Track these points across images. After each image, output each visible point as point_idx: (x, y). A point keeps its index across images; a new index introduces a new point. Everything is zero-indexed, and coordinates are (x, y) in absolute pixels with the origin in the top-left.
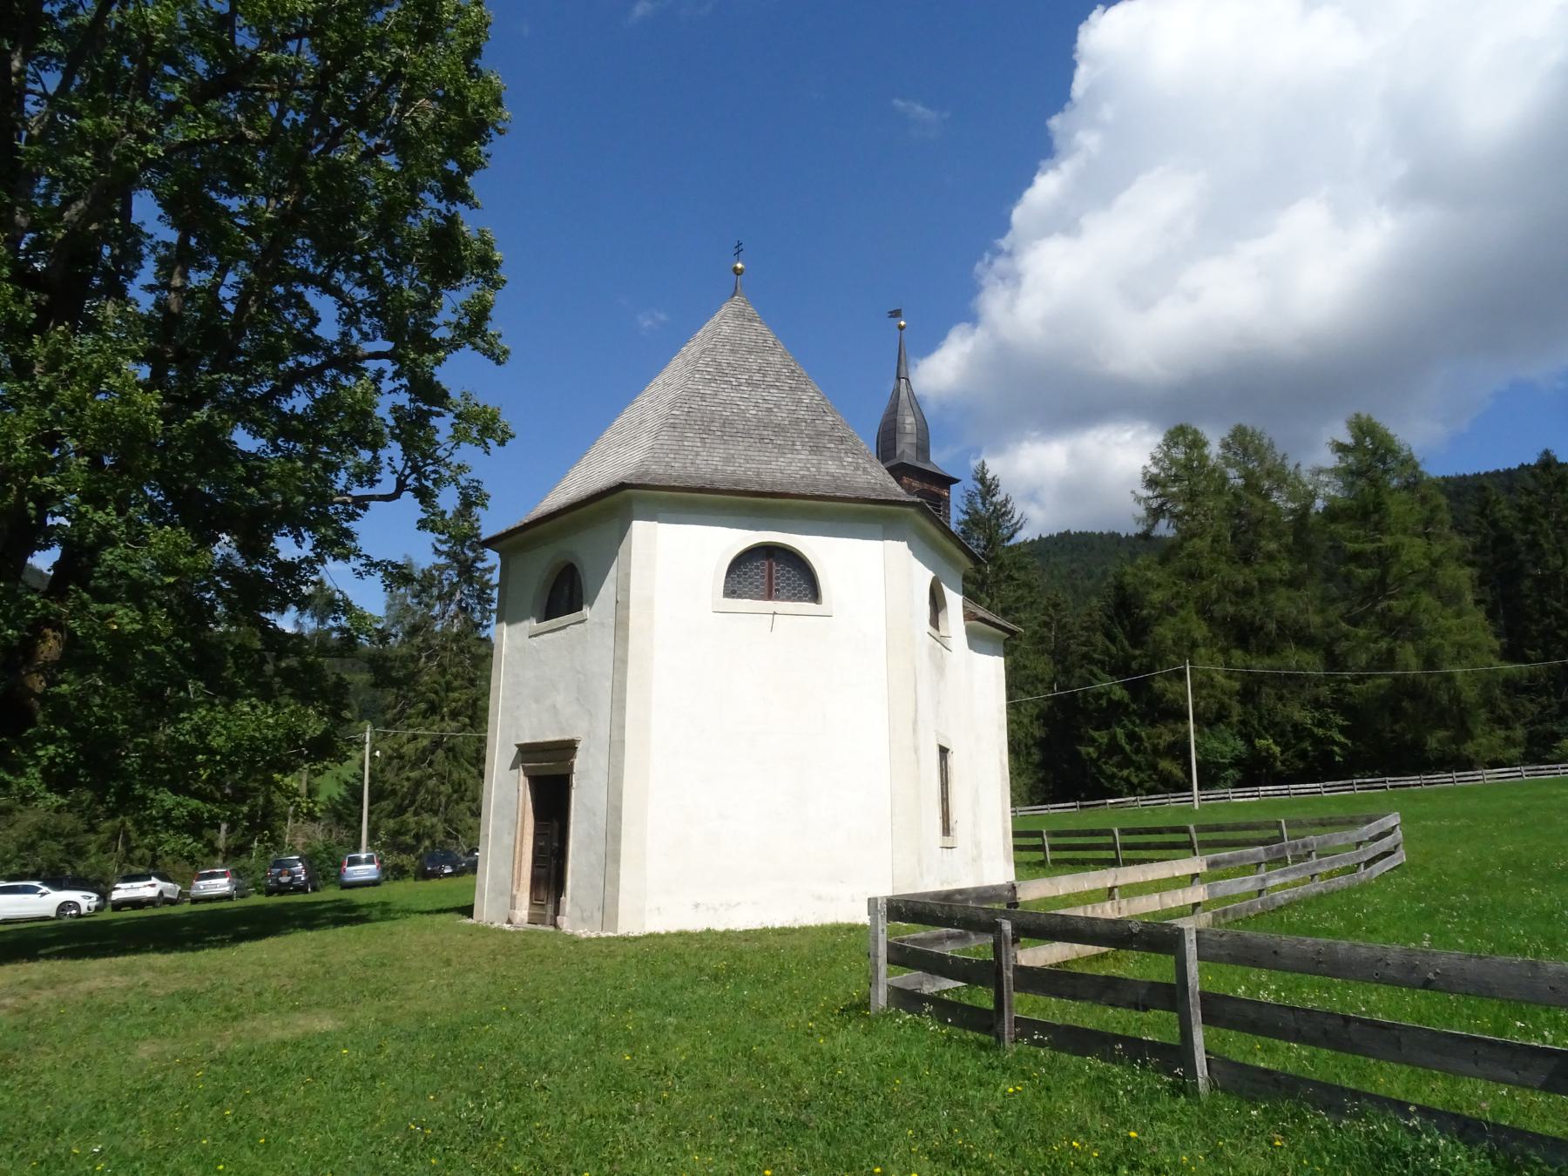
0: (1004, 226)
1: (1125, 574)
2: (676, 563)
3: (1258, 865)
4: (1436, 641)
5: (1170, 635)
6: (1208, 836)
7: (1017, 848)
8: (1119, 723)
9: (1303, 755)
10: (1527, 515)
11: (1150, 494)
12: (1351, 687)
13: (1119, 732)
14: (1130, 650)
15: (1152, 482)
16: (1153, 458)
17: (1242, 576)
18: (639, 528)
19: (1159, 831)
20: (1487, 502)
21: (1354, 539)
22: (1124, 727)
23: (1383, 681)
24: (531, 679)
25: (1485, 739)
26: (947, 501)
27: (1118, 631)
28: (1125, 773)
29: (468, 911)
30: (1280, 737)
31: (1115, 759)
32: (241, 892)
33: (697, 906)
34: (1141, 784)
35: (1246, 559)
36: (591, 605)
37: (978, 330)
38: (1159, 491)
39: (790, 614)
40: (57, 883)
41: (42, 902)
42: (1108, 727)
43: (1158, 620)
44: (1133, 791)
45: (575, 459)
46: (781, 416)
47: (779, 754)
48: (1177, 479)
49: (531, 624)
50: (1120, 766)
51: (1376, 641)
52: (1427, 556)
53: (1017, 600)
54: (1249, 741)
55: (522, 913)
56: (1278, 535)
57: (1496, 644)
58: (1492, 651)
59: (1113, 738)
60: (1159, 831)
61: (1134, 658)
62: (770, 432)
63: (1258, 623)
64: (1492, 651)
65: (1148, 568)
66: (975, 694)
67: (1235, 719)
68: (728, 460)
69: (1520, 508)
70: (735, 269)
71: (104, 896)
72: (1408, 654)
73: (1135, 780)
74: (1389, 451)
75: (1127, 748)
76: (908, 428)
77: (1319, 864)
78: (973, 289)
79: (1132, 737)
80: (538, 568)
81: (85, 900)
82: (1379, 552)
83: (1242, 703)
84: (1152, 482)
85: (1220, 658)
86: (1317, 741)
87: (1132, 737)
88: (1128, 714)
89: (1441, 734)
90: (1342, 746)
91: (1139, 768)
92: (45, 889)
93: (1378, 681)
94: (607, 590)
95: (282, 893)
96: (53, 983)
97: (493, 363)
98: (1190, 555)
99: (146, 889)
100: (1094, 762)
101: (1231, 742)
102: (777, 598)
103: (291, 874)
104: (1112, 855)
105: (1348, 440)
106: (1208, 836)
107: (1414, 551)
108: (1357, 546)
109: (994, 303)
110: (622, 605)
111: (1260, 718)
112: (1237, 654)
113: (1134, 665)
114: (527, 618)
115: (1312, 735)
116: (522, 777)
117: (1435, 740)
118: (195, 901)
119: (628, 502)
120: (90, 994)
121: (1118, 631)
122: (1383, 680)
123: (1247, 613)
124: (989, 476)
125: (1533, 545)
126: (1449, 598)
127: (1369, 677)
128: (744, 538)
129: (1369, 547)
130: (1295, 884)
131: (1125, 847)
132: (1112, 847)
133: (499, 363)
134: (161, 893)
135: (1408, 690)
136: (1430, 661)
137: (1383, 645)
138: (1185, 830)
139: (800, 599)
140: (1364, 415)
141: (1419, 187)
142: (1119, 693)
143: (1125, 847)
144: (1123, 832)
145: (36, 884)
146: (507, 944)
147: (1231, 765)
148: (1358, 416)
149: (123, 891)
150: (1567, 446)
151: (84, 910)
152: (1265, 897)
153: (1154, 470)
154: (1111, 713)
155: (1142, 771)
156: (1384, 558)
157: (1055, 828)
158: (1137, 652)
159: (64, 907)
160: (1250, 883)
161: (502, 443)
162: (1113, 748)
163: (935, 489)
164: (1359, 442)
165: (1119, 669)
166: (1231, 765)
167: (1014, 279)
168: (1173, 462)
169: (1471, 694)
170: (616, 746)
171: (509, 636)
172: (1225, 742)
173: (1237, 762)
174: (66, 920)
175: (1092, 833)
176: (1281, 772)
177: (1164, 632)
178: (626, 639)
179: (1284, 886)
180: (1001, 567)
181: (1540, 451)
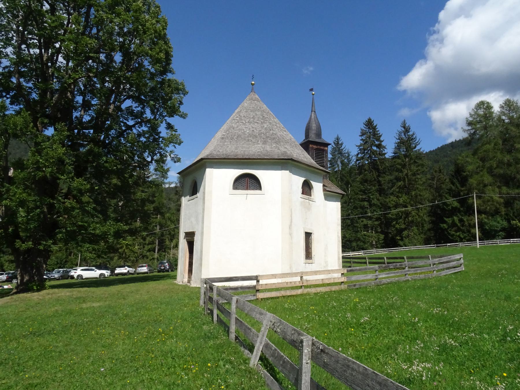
0: (435, 20)
1: (458, 159)
2: (218, 181)
3: (376, 271)
5: (476, 182)
7: (343, 262)
8: (456, 215)
11: (470, 128)
13: (455, 218)
14: (460, 188)
15: (470, 124)
16: (470, 114)
17: (507, 158)
18: (208, 171)
22: (458, 217)
26: (327, 151)
27: (455, 181)
28: (458, 234)
31: (454, 229)
32: (151, 271)
34: (465, 237)
35: (509, 152)
37: (428, 62)
38: (474, 126)
39: (252, 194)
40: (99, 267)
41: (95, 273)
42: (452, 217)
43: (471, 176)
44: (461, 240)
45: (204, 148)
46: (256, 132)
48: (480, 122)
50: (456, 231)
53: (417, 171)
54: (509, 221)
59: (453, 221)
61: (462, 191)
62: (253, 137)
63: (513, 176)
65: (467, 157)
66: (327, 216)
67: (503, 213)
68: (236, 149)
70: (252, 84)
71: (112, 271)
73: (462, 236)
75: (459, 224)
76: (313, 128)
77: (408, 271)
78: (425, 44)
79: (461, 221)
81: (106, 273)
83: (505, 207)
84: (470, 124)
85: (497, 190)
87: (461, 221)
88: (459, 211)
91: (463, 232)
92: (96, 270)
95: (163, 272)
96: (54, 293)
97: (182, 119)
98: (485, 151)
99: (124, 270)
100: (446, 230)
101: (501, 222)
102: (249, 189)
103: (164, 266)
109: (433, 51)
110: (204, 193)
111: (514, 213)
112: (504, 189)
113: (462, 193)
118: (138, 274)
119: (205, 162)
120: (59, 297)
121: (455, 181)
123: (509, 172)
124: (407, 125)
128: (237, 172)
130: (398, 276)
133: (184, 118)
134: (128, 271)
142: (456, 204)
145: (94, 268)
147: (501, 231)
149: (118, 271)
151: (106, 276)
152: (378, 280)
153: (471, 119)
154: (454, 211)
155: (465, 233)
157: (409, 255)
158: (463, 189)
159: (101, 275)
160: (370, 276)
161: (179, 144)
162: (454, 224)
163: (322, 148)
165: (455, 195)
166: (501, 231)
167: (441, 41)
168: (479, 115)
170: (202, 233)
172: (498, 223)
173: (503, 229)
174: (102, 278)
177: (473, 181)
179: (385, 278)
180: (411, 159)
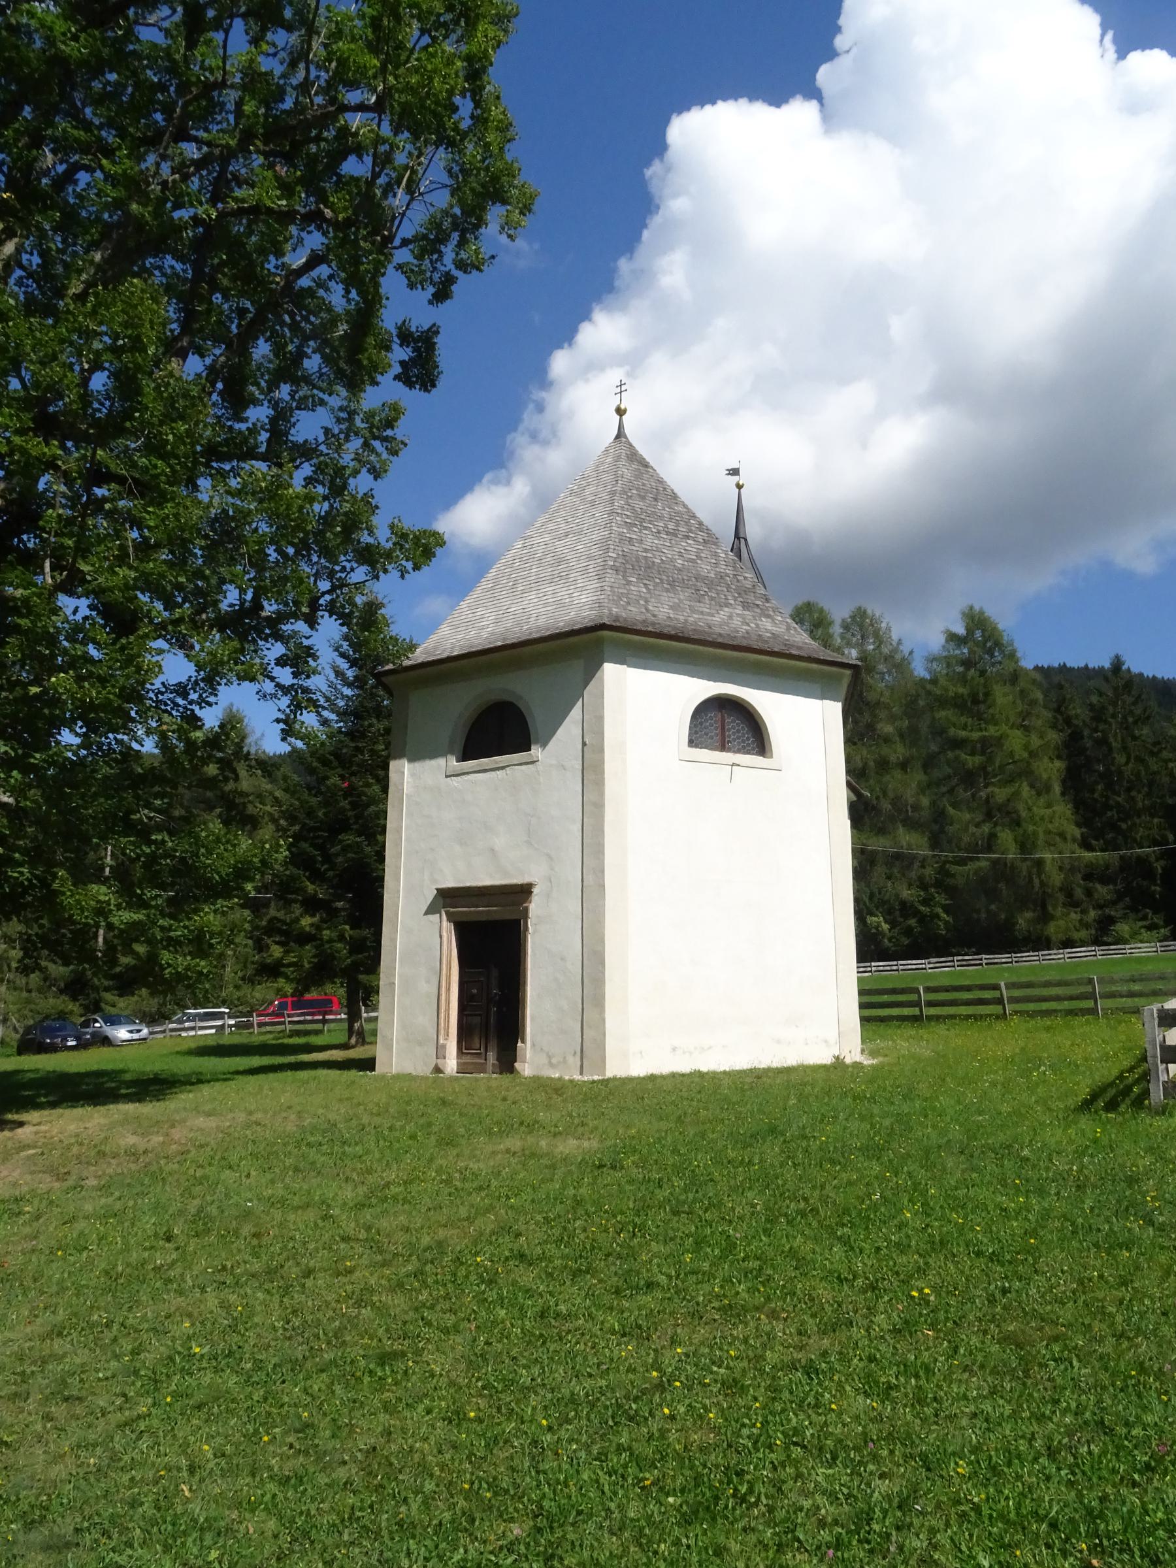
4: (1031, 828)
6: (1017, 993)
9: (908, 932)
10: (1098, 715)
12: (954, 869)
18: (610, 670)
19: (968, 988)
20: (1064, 700)
21: (961, 728)
23: (984, 864)
24: (442, 823)
25: (1063, 921)
29: (368, 1064)
30: (888, 914)
33: (674, 1049)
36: (544, 745)
47: (709, 909)
49: (452, 762)
51: (977, 825)
52: (1026, 747)
55: (451, 1064)
56: (892, 718)
57: (1077, 832)
58: (1074, 840)
60: (968, 988)
64: (1074, 840)
69: (1092, 707)
72: (1006, 837)
74: (998, 644)
80: (459, 704)
82: (984, 741)
86: (922, 919)
89: (1029, 915)
90: (946, 923)
93: (978, 864)
94: (569, 731)
102: (729, 750)
104: (916, 1011)
105: (960, 630)
106: (1017, 993)
107: (1016, 741)
108: (963, 734)
114: (443, 754)
115: (917, 913)
116: (445, 923)
117: (1024, 920)
122: (983, 863)
125: (1103, 742)
126: (1042, 789)
127: (971, 859)
128: (705, 689)
129: (976, 735)
131: (930, 1004)
132: (917, 1004)
135: (1002, 871)
136: (1025, 846)
137: (986, 828)
138: (996, 987)
139: (748, 753)
140: (977, 608)
141: (953, 389)
143: (930, 1004)
144: (928, 990)
146: (422, 1100)
148: (971, 608)
150: (1162, 658)
156: (986, 746)
164: (970, 631)
169: (1057, 879)
171: (412, 775)
175: (894, 991)
176: (888, 949)
178: (600, 783)
181: (1112, 655)
